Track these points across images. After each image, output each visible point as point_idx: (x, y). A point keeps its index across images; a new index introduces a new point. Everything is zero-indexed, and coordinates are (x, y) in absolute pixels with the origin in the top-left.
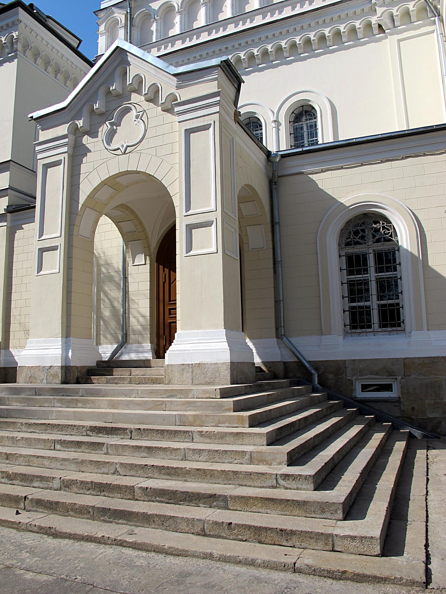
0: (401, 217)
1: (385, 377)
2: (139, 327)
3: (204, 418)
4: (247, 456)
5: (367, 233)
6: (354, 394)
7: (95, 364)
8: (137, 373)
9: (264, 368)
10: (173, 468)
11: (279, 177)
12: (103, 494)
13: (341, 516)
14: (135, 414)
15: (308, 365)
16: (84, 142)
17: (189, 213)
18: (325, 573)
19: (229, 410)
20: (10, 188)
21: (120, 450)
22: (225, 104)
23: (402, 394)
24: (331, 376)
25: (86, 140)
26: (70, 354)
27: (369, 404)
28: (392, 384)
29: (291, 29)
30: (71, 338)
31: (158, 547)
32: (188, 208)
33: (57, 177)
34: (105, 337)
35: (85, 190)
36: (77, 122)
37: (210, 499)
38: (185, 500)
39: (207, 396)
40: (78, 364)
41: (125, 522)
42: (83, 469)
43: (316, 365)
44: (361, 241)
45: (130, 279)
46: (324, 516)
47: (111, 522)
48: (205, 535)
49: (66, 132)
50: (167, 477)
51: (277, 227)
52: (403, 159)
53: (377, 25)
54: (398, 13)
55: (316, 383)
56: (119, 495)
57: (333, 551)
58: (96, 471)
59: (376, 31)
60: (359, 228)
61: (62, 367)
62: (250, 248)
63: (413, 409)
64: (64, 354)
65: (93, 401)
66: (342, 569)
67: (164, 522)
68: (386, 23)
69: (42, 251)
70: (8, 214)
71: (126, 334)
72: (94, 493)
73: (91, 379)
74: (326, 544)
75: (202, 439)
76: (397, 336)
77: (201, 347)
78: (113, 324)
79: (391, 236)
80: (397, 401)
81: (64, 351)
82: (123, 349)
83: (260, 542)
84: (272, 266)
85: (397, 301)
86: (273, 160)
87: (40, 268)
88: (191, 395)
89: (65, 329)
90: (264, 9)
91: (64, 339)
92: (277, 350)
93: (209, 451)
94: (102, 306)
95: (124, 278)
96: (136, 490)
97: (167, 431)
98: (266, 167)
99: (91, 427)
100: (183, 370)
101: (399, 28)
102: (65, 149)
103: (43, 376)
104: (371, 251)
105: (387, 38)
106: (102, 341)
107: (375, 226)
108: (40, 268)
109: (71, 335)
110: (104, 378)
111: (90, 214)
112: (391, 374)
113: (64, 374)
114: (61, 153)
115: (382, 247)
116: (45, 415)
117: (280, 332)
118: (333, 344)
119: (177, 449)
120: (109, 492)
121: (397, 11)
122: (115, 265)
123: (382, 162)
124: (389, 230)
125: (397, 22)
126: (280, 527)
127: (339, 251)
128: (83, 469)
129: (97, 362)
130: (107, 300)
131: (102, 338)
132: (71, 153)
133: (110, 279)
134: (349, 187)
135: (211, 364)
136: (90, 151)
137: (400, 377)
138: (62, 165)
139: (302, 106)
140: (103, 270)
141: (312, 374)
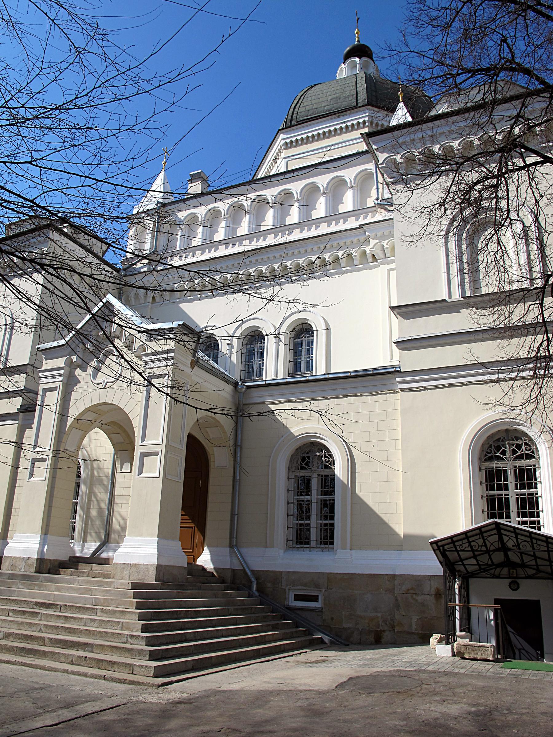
0: (337, 448)
1: (312, 589)
2: (119, 528)
3: (110, 601)
4: (120, 625)
5: (311, 460)
6: (286, 603)
7: (67, 559)
8: (96, 568)
9: (215, 573)
10: (73, 628)
11: (244, 405)
12: (27, 642)
13: (148, 658)
14: (68, 596)
15: (249, 573)
16: (76, 374)
17: (143, 443)
18: (117, 680)
19: (130, 597)
20: (25, 389)
21: (49, 618)
22: (180, 357)
23: (324, 604)
24: (269, 585)
25: (78, 372)
26: (45, 549)
27: (298, 612)
28: (318, 596)
29: (296, 252)
30: (48, 536)
31: (42, 666)
32: (143, 440)
33: (53, 399)
34: (91, 535)
35: (74, 411)
36: (72, 357)
37: (84, 646)
38: (71, 646)
39: (123, 587)
40: (52, 558)
41: (33, 656)
42: (21, 628)
43: (258, 574)
44: (306, 467)
45: (117, 485)
46: (140, 658)
47: (25, 656)
48: (73, 664)
49: (63, 365)
50: (69, 634)
51: (239, 449)
52: (344, 397)
53: (370, 255)
54: (388, 246)
55: (255, 589)
56: (36, 643)
57: (132, 674)
58: (29, 629)
59: (370, 259)
60: (306, 455)
61: (37, 559)
62: (216, 466)
63: (332, 619)
64: (41, 549)
65: (45, 586)
66: (125, 678)
67: (53, 656)
68: (379, 254)
69: (34, 461)
70: (21, 414)
71: (109, 534)
72: (22, 641)
73: (59, 571)
74: (130, 670)
75: (102, 614)
76: (303, 552)
77: (139, 551)
78: (98, 523)
79: (330, 464)
80: (320, 611)
81: (41, 546)
82: (104, 548)
83: (99, 668)
84: (231, 483)
85: (331, 522)
86: (239, 391)
87: (31, 475)
88: (113, 586)
89: (45, 527)
90: (276, 230)
91: (43, 536)
92: (228, 558)
93: (100, 620)
94: (91, 507)
95: (111, 483)
96: (46, 639)
97: (82, 607)
98: (233, 397)
99: (36, 602)
100: (124, 568)
101: (389, 259)
102: (61, 378)
103: (22, 565)
104: (315, 475)
105: (379, 266)
106: (88, 539)
107: (318, 454)
108: (31, 475)
109: (49, 533)
110: (69, 571)
111: (77, 433)
112: (317, 586)
113: (38, 565)
114: (58, 382)
115: (326, 472)
116: (11, 593)
117: (234, 542)
118: (274, 557)
119: (82, 618)
120: (31, 641)
121: (387, 244)
122: (106, 470)
123: (327, 399)
124: (329, 459)
125: (388, 253)
126: (110, 660)
127: (288, 473)
128: (21, 628)
129: (70, 557)
130: (95, 502)
131: (88, 536)
132: (65, 381)
133: (100, 481)
134: (300, 419)
135: (144, 565)
136: (80, 382)
137: (324, 590)
138: (57, 392)
139: (303, 324)
140: (96, 473)
141: (251, 582)
